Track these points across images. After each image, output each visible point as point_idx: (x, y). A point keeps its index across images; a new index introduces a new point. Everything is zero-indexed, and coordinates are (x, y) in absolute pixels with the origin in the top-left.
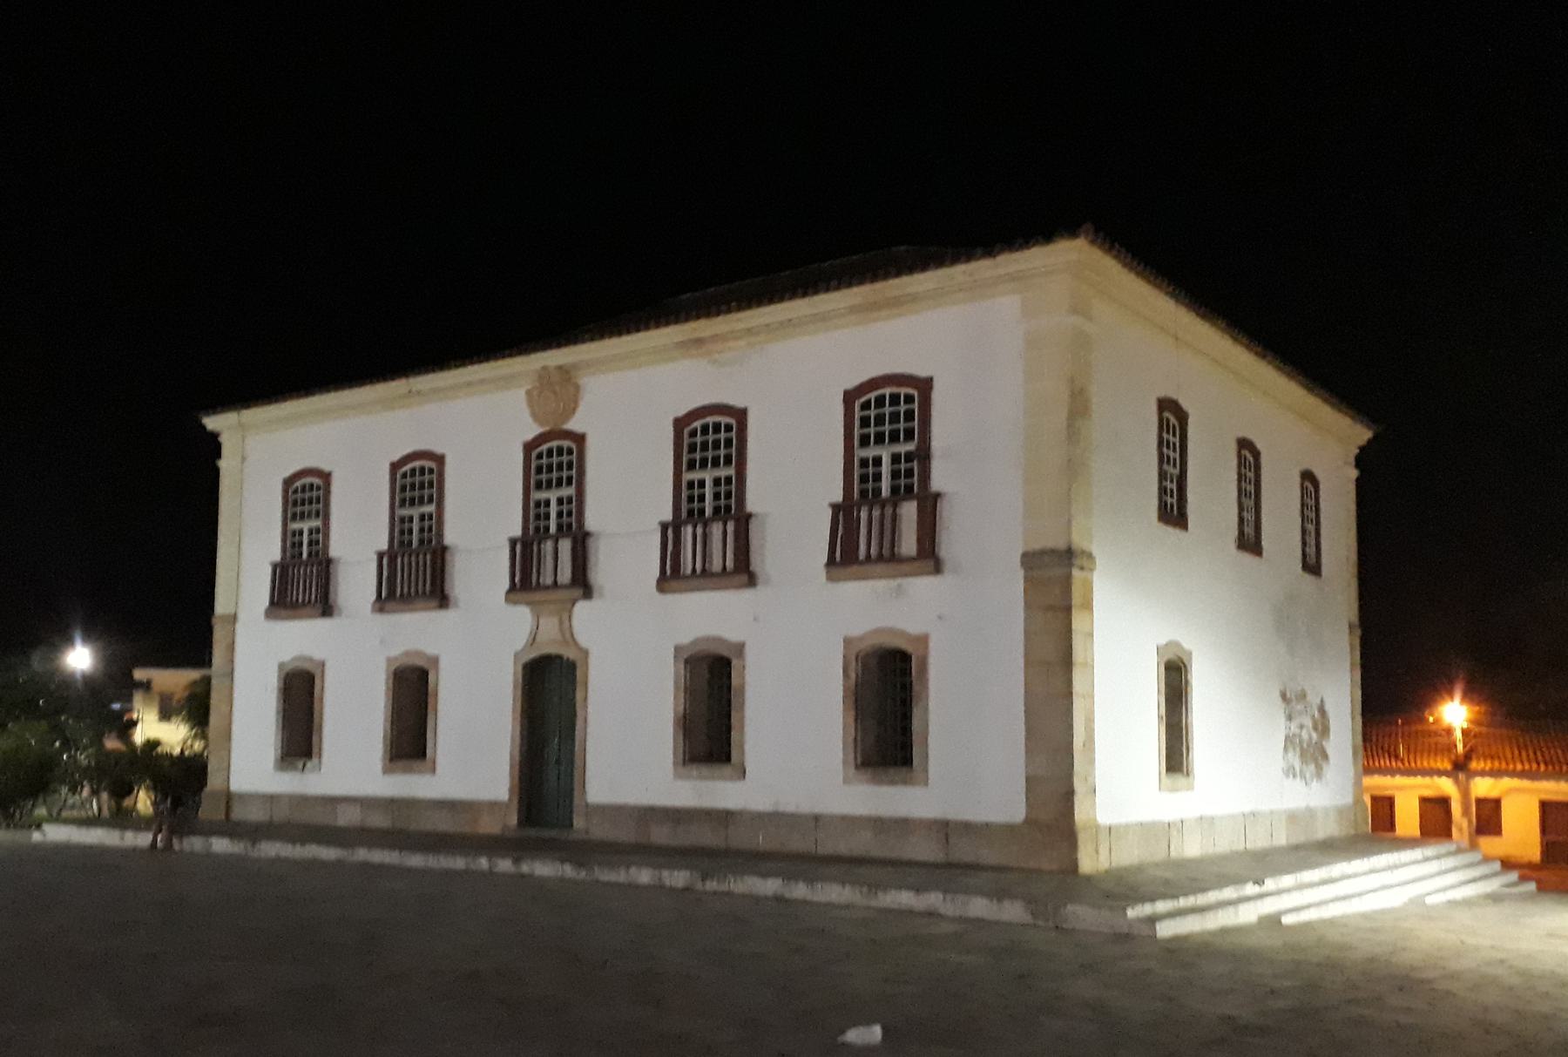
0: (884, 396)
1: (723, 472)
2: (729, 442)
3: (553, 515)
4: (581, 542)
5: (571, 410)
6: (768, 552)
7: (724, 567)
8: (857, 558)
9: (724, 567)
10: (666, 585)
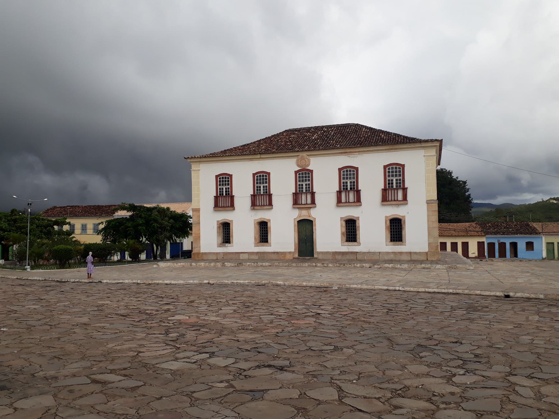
5: (308, 165)
9: (354, 201)
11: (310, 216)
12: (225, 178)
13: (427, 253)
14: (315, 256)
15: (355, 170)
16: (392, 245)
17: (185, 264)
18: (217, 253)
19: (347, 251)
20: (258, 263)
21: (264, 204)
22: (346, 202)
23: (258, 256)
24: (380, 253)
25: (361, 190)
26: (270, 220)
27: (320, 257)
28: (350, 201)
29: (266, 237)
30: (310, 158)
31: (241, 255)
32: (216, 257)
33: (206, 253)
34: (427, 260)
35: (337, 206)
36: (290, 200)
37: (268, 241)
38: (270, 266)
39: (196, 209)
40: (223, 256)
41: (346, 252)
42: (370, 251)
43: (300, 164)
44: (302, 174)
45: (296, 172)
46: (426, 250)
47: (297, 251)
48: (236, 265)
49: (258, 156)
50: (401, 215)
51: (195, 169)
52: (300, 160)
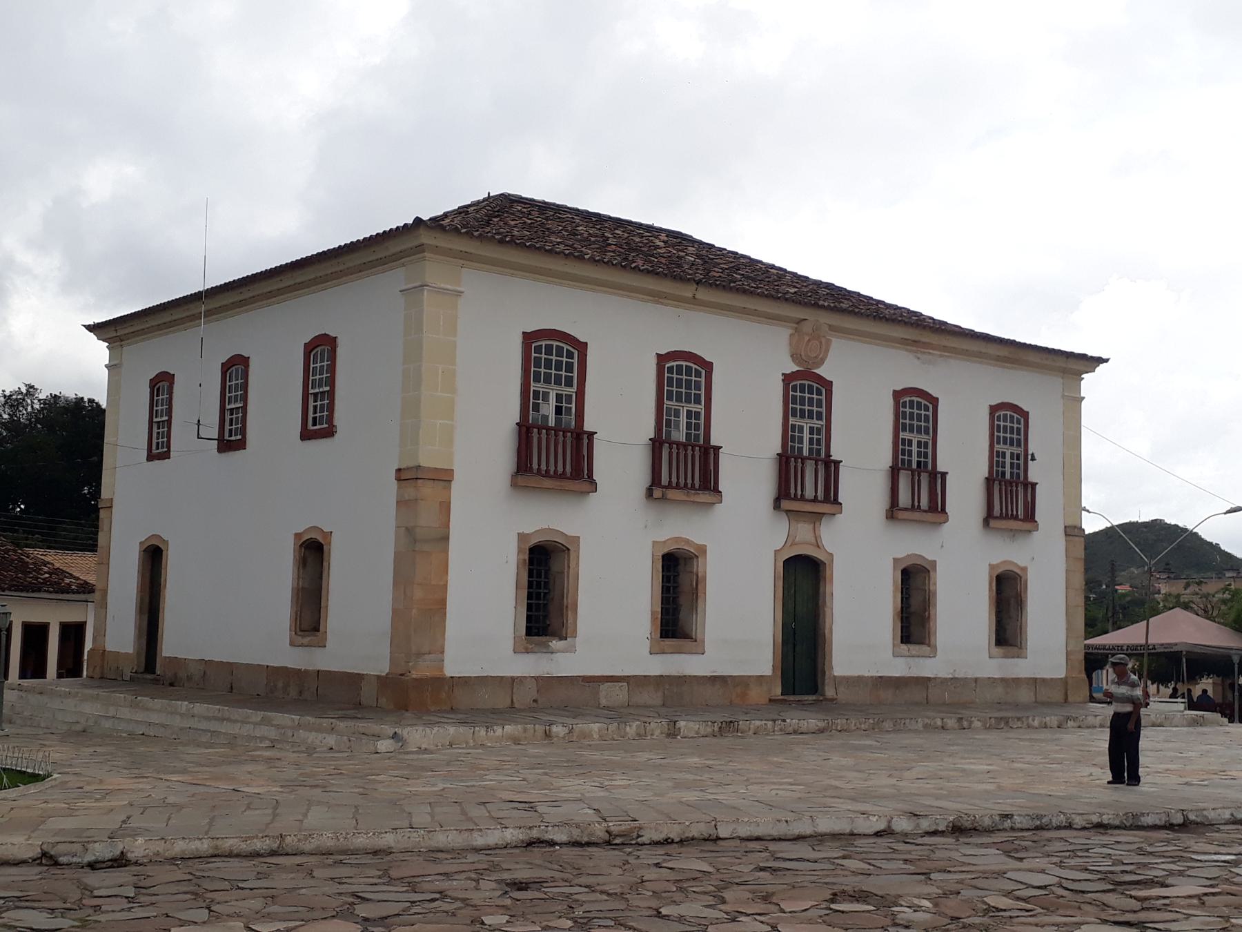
9: (816, 496)
11: (818, 546)
12: (560, 351)
13: (1065, 682)
14: (830, 692)
15: (576, 353)
17: (525, 730)
18: (513, 679)
20: (784, 721)
21: (678, 483)
22: (913, 508)
23: (660, 694)
26: (703, 550)
27: (843, 695)
31: (601, 686)
33: (465, 681)
34: (1066, 700)
35: (514, 485)
38: (821, 731)
42: (956, 676)
43: (802, 353)
45: (787, 378)
46: (1061, 674)
47: (779, 673)
48: (716, 729)
49: (688, 291)
52: (807, 338)
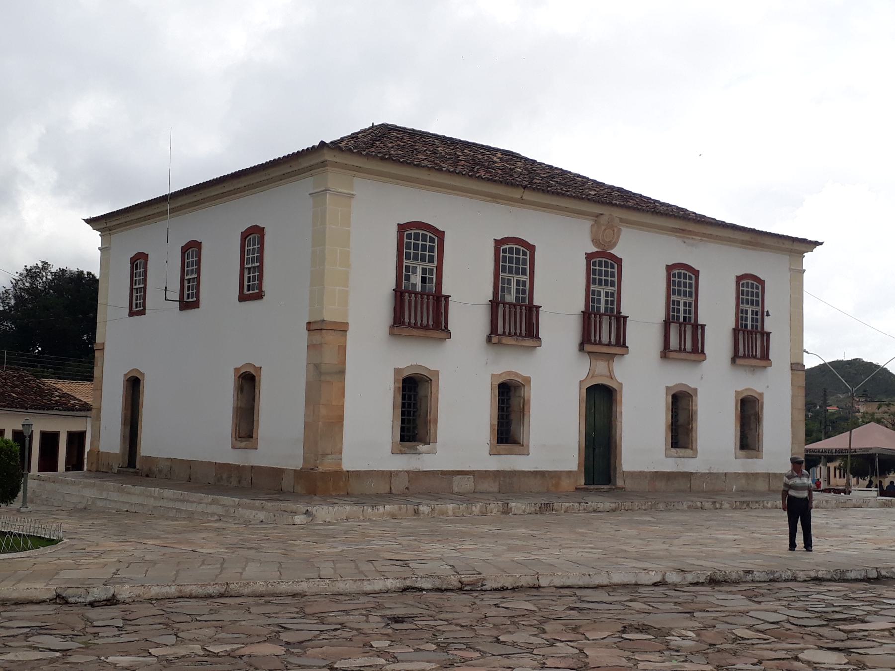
0: (675, 274)
1: (610, 289)
2: (504, 261)
3: (682, 311)
4: (620, 321)
5: (613, 245)
6: (456, 318)
7: (610, 342)
8: (698, 352)
9: (610, 342)
10: (739, 361)
12: (424, 238)
14: (619, 483)
16: (744, 458)
17: (400, 509)
18: (391, 472)
19: (674, 470)
22: (680, 351)
24: (726, 474)
25: (705, 325)
26: (527, 380)
27: (629, 485)
28: (603, 342)
29: (406, 426)
30: (622, 228)
32: (388, 487)
33: (358, 474)
35: (392, 334)
36: (572, 332)
37: (401, 432)
39: (335, 322)
40: (407, 484)
41: (673, 472)
42: (712, 471)
44: (417, 236)
45: (589, 257)
47: (583, 469)
48: (538, 509)
49: (517, 193)
50: (758, 390)
51: (340, 190)
